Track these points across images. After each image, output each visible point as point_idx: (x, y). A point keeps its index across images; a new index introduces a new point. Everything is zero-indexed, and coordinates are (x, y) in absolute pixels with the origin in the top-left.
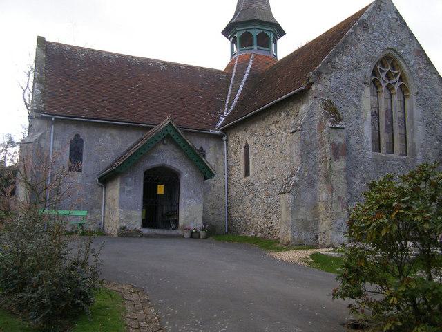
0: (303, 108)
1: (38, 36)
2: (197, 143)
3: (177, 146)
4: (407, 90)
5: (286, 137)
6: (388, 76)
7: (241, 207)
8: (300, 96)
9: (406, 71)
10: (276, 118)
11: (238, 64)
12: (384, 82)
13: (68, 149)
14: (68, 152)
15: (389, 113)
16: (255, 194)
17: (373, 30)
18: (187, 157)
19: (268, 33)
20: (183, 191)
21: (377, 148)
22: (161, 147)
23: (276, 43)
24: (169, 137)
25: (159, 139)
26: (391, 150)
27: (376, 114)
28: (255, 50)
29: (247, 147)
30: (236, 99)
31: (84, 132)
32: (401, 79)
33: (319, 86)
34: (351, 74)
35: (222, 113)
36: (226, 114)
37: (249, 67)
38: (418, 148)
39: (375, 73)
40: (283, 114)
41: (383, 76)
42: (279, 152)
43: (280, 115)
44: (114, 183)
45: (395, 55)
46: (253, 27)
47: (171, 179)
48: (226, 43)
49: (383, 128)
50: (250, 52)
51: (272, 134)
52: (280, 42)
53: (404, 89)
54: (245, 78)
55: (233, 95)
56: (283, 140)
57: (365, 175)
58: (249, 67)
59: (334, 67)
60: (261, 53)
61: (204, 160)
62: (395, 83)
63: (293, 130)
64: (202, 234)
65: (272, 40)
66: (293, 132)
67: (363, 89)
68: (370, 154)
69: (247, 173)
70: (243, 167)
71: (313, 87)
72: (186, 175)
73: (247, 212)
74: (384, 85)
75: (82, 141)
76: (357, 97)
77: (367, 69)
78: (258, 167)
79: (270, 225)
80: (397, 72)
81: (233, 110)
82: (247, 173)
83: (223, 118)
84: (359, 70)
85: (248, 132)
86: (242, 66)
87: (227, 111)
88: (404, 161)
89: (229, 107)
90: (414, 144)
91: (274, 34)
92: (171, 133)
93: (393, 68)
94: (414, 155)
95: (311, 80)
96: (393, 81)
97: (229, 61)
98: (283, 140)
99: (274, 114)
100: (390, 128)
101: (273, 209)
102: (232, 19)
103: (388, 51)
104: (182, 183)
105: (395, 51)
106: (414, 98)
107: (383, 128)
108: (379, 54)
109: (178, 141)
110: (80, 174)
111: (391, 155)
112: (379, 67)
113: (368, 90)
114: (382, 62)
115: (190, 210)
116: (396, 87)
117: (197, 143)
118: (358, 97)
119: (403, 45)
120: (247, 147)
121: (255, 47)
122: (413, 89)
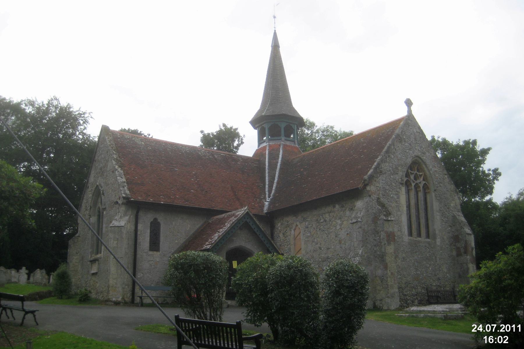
0: (359, 204)
1: (103, 126)
4: (428, 188)
5: (341, 225)
8: (355, 194)
9: (428, 173)
10: (329, 208)
11: (270, 153)
12: (414, 182)
13: (149, 231)
14: (149, 234)
17: (405, 141)
21: (410, 234)
26: (419, 235)
27: (409, 207)
28: (282, 142)
30: (274, 188)
31: (161, 218)
32: (424, 180)
33: (372, 187)
34: (392, 176)
35: (265, 198)
36: (268, 200)
37: (280, 156)
38: (437, 232)
39: (407, 175)
41: (412, 177)
43: (334, 207)
45: (420, 161)
46: (278, 119)
49: (414, 219)
51: (325, 221)
54: (278, 167)
56: (338, 227)
57: (404, 255)
58: (280, 156)
59: (381, 172)
61: (272, 242)
62: (420, 183)
63: (354, 221)
66: (354, 223)
67: (400, 188)
68: (406, 238)
74: (413, 185)
75: (159, 224)
76: (396, 194)
77: (401, 174)
80: (421, 174)
81: (274, 195)
83: (267, 203)
84: (397, 174)
85: (300, 217)
87: (269, 197)
88: (429, 243)
89: (271, 187)
90: (435, 230)
92: (248, 221)
93: (418, 171)
94: (435, 238)
96: (418, 181)
97: (256, 148)
98: (338, 227)
103: (416, 158)
105: (420, 158)
106: (433, 194)
108: (409, 161)
109: (253, 227)
110: (158, 253)
111: (420, 239)
112: (409, 171)
113: (403, 189)
114: (411, 167)
116: (421, 186)
118: (398, 194)
119: (424, 153)
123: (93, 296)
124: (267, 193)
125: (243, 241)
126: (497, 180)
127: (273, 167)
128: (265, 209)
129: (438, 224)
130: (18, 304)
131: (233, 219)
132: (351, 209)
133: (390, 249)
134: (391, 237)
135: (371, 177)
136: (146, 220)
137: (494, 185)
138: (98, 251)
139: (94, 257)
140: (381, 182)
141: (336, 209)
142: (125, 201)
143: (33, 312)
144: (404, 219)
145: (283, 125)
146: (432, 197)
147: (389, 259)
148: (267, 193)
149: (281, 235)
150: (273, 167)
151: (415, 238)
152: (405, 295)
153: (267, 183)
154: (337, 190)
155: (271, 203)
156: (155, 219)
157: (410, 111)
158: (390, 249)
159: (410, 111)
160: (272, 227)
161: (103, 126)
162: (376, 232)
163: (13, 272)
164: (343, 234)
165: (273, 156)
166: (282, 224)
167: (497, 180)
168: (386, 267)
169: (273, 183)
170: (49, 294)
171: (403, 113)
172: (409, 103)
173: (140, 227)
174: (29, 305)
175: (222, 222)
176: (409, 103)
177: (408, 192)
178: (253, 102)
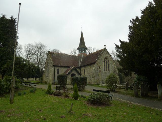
6: (106, 60)
8: (94, 63)
10: (90, 66)
15: (106, 65)
21: (105, 70)
26: (107, 71)
27: (105, 65)
29: (85, 70)
31: (59, 68)
39: (104, 60)
41: (105, 60)
46: (82, 47)
49: (106, 68)
53: (108, 62)
64: (81, 96)
68: (104, 71)
69: (85, 74)
70: (84, 73)
75: (59, 69)
77: (103, 59)
82: (85, 74)
86: (81, 54)
89: (80, 61)
100: (107, 68)
107: (106, 68)
114: (105, 58)
116: (107, 61)
120: (85, 70)
122: (109, 62)
123: (47, 83)
125: (74, 72)
126: (137, 17)
127: (81, 58)
128: (79, 66)
129: (111, 68)
130: (33, 85)
131: (72, 68)
132: (93, 66)
133: (100, 74)
134: (100, 71)
135: (97, 60)
136: (56, 68)
137: (140, 15)
138: (48, 75)
139: (47, 75)
140: (99, 61)
143: (36, 86)
144: (103, 68)
146: (109, 63)
147: (100, 75)
150: (81, 58)
151: (106, 71)
154: (91, 63)
155: (80, 65)
157: (105, 47)
158: (100, 74)
159: (105, 47)
160: (80, 70)
162: (97, 70)
163: (32, 78)
164: (92, 71)
165: (81, 56)
167: (137, 17)
168: (99, 77)
169: (81, 59)
170: (39, 83)
171: (104, 48)
172: (105, 46)
173: (55, 70)
174: (35, 85)
175: (70, 69)
176: (105, 46)
177: (104, 63)
178: (78, 45)
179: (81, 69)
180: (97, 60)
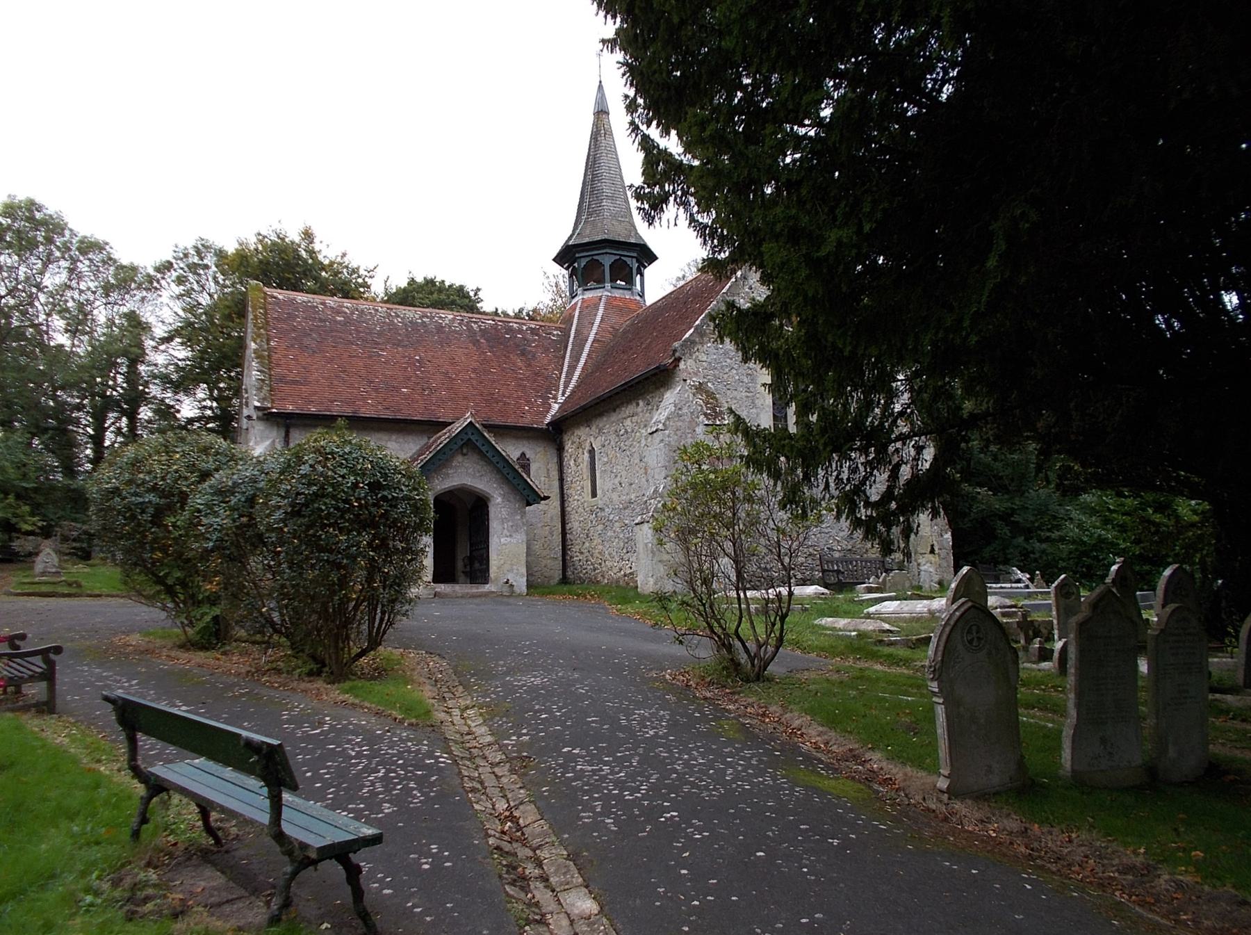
0: (670, 398)
1: (554, 260)
2: (512, 450)
3: (482, 455)
7: (587, 544)
10: (630, 409)
16: (607, 524)
18: (499, 471)
19: (628, 261)
20: (495, 526)
22: (460, 458)
23: (642, 275)
24: (470, 443)
25: (456, 447)
29: (592, 452)
30: (575, 378)
33: (690, 362)
35: (555, 398)
36: (561, 399)
40: (641, 403)
42: (637, 461)
43: (638, 404)
44: (410, 438)
47: (478, 507)
48: (561, 273)
50: (598, 293)
51: (626, 432)
52: (649, 271)
55: (576, 359)
56: (643, 442)
60: (617, 294)
65: (634, 271)
69: (594, 494)
71: (682, 365)
72: (499, 500)
73: (596, 554)
78: (609, 485)
79: (628, 571)
81: (573, 392)
82: (594, 494)
83: (556, 406)
89: (566, 387)
91: (638, 261)
92: (473, 438)
95: (677, 354)
99: (629, 402)
101: (629, 546)
102: (570, 238)
104: (493, 511)
109: (484, 449)
115: (508, 548)
117: (512, 450)
121: (608, 285)
124: (561, 387)
135: (691, 342)
141: (639, 409)
142: (260, 414)
145: (607, 261)
148: (561, 387)
149: (572, 463)
152: (766, 569)
153: (565, 369)
156: (523, 454)
160: (560, 449)
161: (554, 260)
166: (573, 443)
169: (578, 361)
179: (569, 448)
180: (691, 342)
